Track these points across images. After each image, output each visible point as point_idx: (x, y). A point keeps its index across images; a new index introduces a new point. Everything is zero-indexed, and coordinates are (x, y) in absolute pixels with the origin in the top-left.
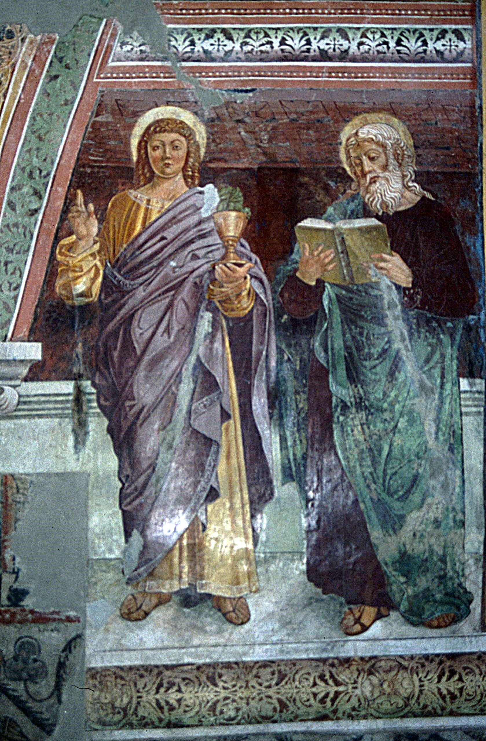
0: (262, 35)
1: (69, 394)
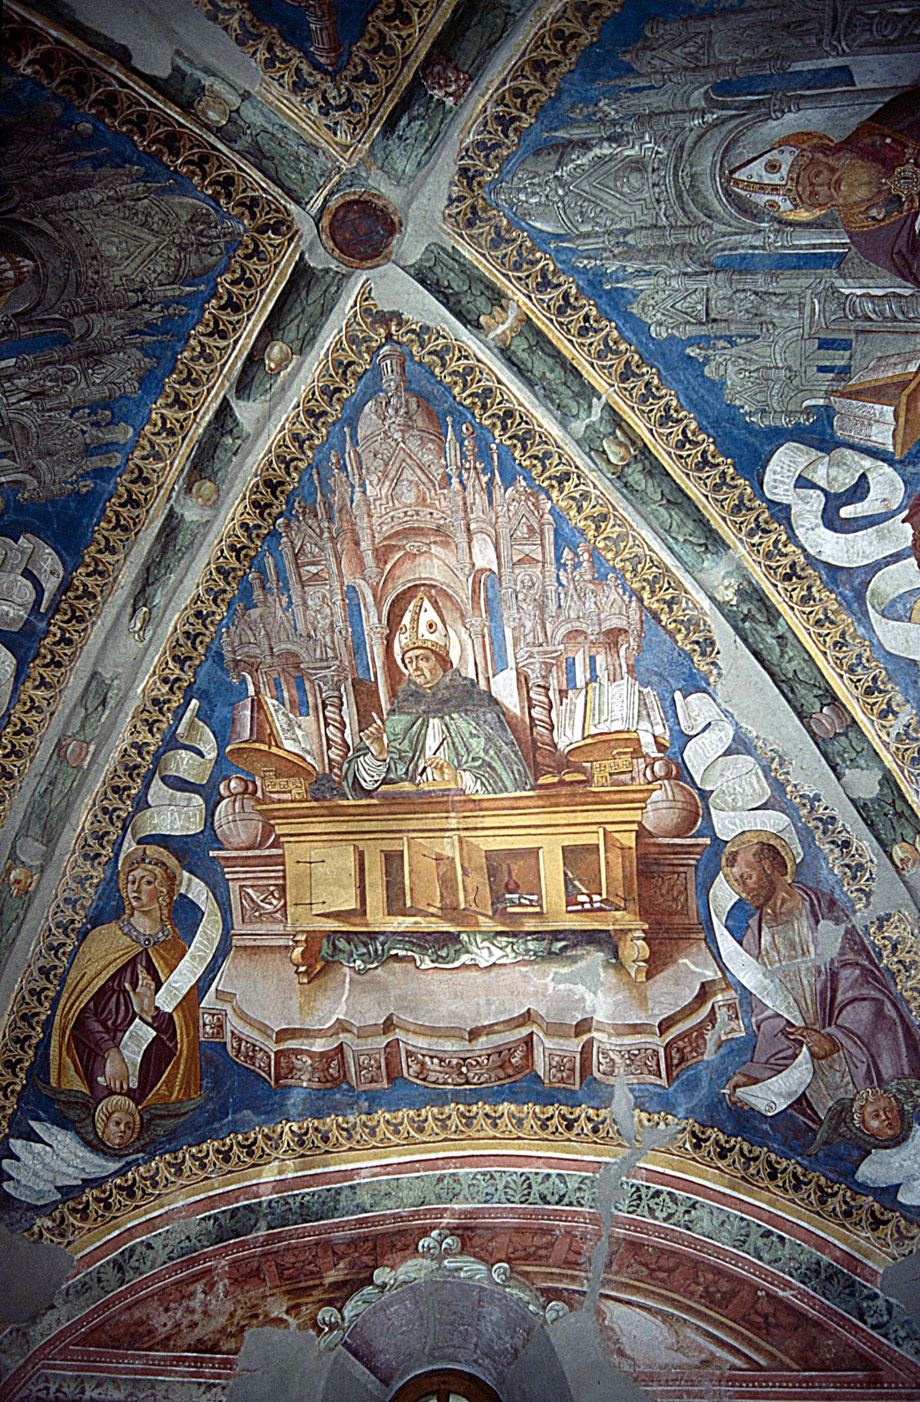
1: (59, 1082)
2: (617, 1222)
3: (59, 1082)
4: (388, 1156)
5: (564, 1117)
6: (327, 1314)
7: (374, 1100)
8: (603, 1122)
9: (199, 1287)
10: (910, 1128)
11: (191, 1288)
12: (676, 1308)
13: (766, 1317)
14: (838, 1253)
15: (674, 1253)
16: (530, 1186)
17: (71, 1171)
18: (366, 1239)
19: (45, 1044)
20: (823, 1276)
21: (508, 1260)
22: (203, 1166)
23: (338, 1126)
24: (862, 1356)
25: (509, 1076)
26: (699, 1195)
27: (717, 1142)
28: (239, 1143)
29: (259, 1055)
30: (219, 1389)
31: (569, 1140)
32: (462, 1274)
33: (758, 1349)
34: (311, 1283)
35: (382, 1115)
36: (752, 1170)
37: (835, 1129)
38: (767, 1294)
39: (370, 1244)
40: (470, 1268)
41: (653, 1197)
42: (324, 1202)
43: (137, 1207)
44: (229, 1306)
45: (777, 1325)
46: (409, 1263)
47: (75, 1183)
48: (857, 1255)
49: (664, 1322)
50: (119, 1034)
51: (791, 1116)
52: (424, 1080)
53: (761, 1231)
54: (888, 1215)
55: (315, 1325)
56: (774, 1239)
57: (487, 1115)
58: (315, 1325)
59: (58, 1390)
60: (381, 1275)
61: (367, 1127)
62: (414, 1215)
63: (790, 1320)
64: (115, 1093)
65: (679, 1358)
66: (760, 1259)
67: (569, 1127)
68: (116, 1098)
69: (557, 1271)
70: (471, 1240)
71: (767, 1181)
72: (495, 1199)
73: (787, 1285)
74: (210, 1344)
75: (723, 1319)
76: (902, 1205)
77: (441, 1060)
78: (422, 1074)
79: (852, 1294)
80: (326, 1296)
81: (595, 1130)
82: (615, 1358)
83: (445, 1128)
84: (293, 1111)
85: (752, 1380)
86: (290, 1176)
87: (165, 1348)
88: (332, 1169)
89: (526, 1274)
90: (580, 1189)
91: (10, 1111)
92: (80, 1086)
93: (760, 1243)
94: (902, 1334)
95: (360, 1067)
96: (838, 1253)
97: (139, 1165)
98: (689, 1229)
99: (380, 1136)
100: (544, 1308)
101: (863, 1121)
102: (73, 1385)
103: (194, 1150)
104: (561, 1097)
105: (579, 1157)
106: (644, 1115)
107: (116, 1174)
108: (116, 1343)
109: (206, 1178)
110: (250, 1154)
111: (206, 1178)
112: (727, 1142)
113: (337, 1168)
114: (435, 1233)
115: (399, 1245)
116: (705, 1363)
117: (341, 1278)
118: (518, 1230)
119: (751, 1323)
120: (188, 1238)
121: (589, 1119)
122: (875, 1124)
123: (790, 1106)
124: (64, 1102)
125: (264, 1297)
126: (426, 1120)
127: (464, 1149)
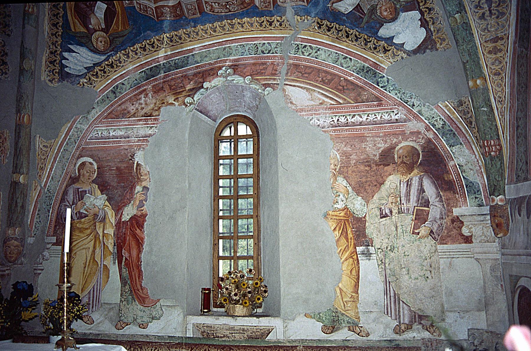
0: (373, 115)
1: (75, 29)
2: (290, 58)
3: (75, 29)
4: (204, 42)
5: (268, 21)
6: (188, 100)
7: (196, 22)
8: (283, 22)
9: (143, 96)
10: (399, 14)
11: (140, 97)
12: (311, 86)
13: (343, 87)
14: (371, 63)
15: (311, 67)
16: (258, 48)
17: (88, 61)
18: (199, 73)
19: (65, 15)
20: (365, 71)
21: (251, 75)
22: (136, 54)
23: (184, 33)
24: (376, 97)
25: (246, 7)
26: (320, 46)
27: (327, 25)
28: (148, 44)
29: (149, 10)
30: (154, 128)
31: (271, 29)
32: (235, 82)
33: (340, 97)
34: (181, 90)
35: (200, 27)
36: (340, 35)
37: (371, 17)
38: (344, 79)
39: (201, 74)
40: (238, 79)
41: (303, 48)
42: (183, 62)
43: (115, 71)
44: (154, 101)
45: (347, 89)
46: (216, 79)
47: (91, 65)
48: (378, 63)
49: (307, 91)
50: (93, 8)
51: (354, 13)
52: (213, 12)
53: (343, 57)
54: (390, 48)
55: (184, 104)
56: (348, 59)
57: (239, 23)
58: (184, 104)
59: (102, 134)
60: (206, 85)
61: (195, 32)
62: (216, 63)
63: (352, 87)
64: (97, 31)
65: (313, 103)
66: (343, 67)
67: (271, 25)
68: (98, 32)
69: (268, 77)
70: (237, 69)
71: (345, 38)
72: (245, 54)
73: (352, 75)
74: (149, 114)
75: (328, 89)
76: (395, 43)
77: (219, 4)
78: (212, 10)
79: (375, 77)
80: (188, 94)
81: (281, 25)
82: (290, 105)
83: (224, 30)
84: (166, 29)
85: (338, 108)
86: (169, 53)
87: (135, 117)
88: (184, 49)
89: (257, 79)
90: (276, 47)
91: (60, 43)
92: (83, 30)
93: (343, 61)
94: (392, 89)
95: (188, 10)
96: (371, 63)
97: (113, 56)
98: (317, 58)
99: (200, 35)
100: (264, 90)
101: (381, 13)
102: (106, 132)
103: (132, 48)
104: (266, 13)
105: (276, 36)
106: (299, 17)
107: (105, 60)
108: (117, 117)
109: (138, 58)
110: (153, 47)
111: (138, 58)
112: (330, 25)
113: (186, 49)
114: (224, 68)
115: (211, 74)
116: (321, 104)
117: (192, 87)
118: (254, 64)
119: (338, 89)
120: (136, 80)
121: (278, 21)
122: (385, 14)
123: (353, 9)
124: (79, 37)
125: (166, 96)
126: (216, 27)
127: (232, 37)
